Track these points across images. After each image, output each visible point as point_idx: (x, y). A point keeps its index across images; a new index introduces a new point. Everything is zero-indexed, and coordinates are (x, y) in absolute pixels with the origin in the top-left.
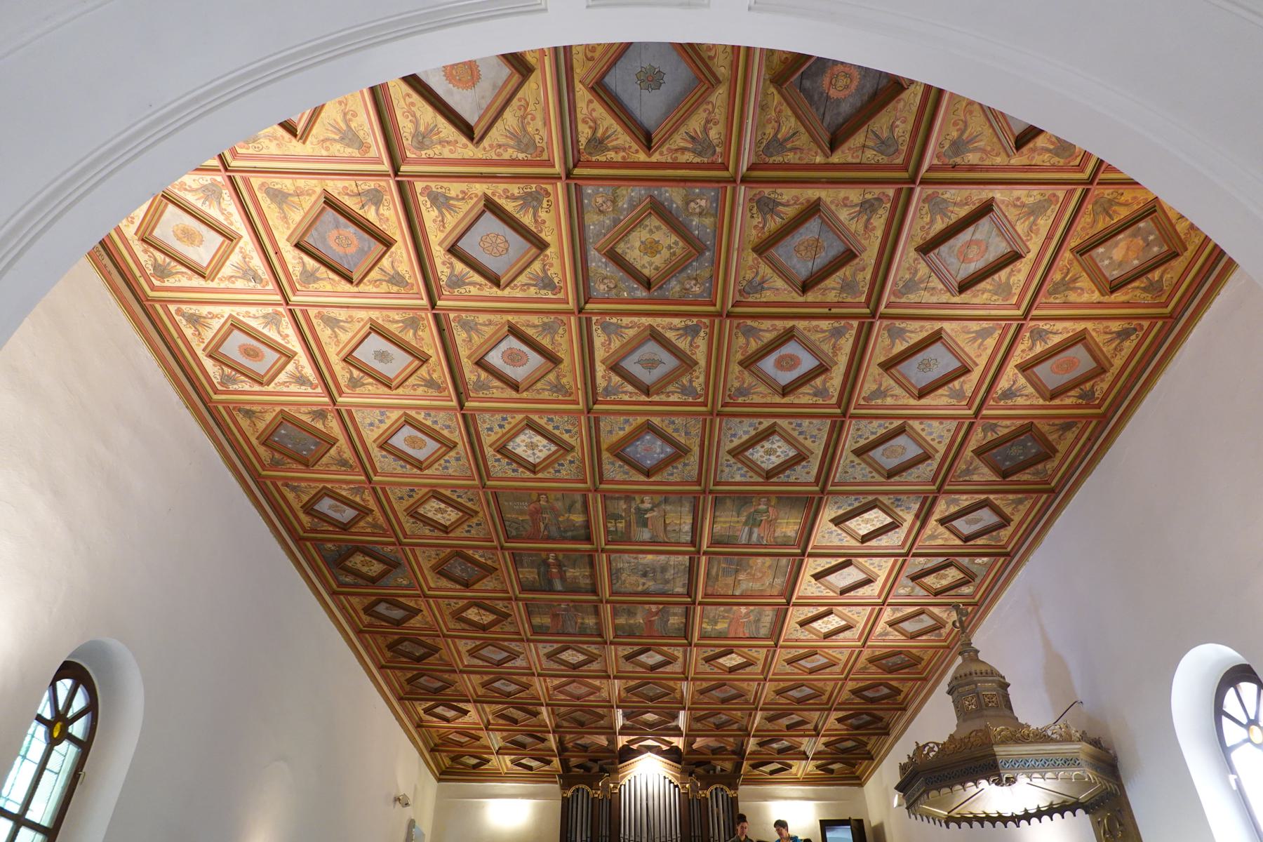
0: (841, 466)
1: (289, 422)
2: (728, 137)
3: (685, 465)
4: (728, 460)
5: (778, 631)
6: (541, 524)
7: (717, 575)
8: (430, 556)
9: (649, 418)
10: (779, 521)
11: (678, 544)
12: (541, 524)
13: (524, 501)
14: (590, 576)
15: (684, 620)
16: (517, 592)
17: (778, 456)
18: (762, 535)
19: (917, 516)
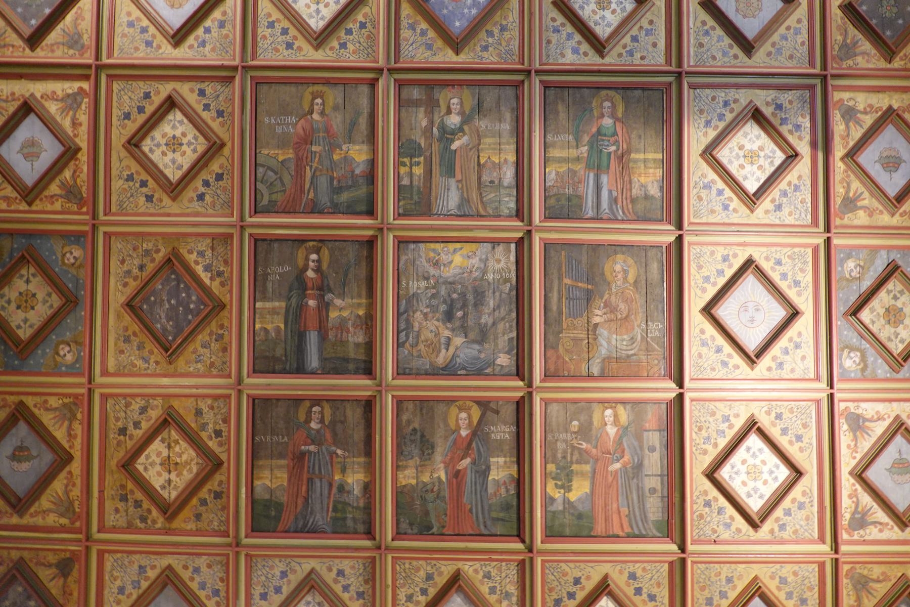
0: (691, 31)
1: (25, 579)
2: (521, 57)
3: (503, 29)
4: (554, 20)
5: (677, 499)
6: (308, 168)
7: (560, 313)
8: (129, 562)
9: (455, 58)
10: (633, 155)
11: (498, 217)
12: (308, 168)
13: (291, 114)
14: (365, 508)
15: (514, 470)
16: (243, 533)
17: (614, 12)
18: (615, 194)
19: (814, 145)
